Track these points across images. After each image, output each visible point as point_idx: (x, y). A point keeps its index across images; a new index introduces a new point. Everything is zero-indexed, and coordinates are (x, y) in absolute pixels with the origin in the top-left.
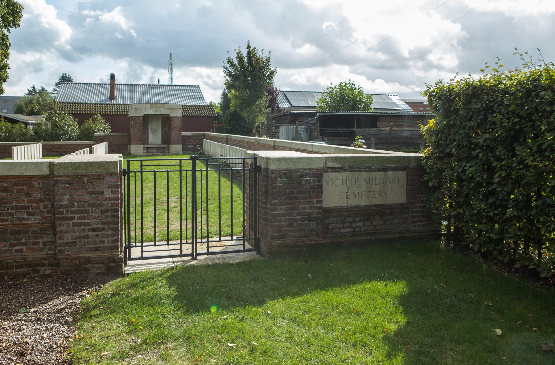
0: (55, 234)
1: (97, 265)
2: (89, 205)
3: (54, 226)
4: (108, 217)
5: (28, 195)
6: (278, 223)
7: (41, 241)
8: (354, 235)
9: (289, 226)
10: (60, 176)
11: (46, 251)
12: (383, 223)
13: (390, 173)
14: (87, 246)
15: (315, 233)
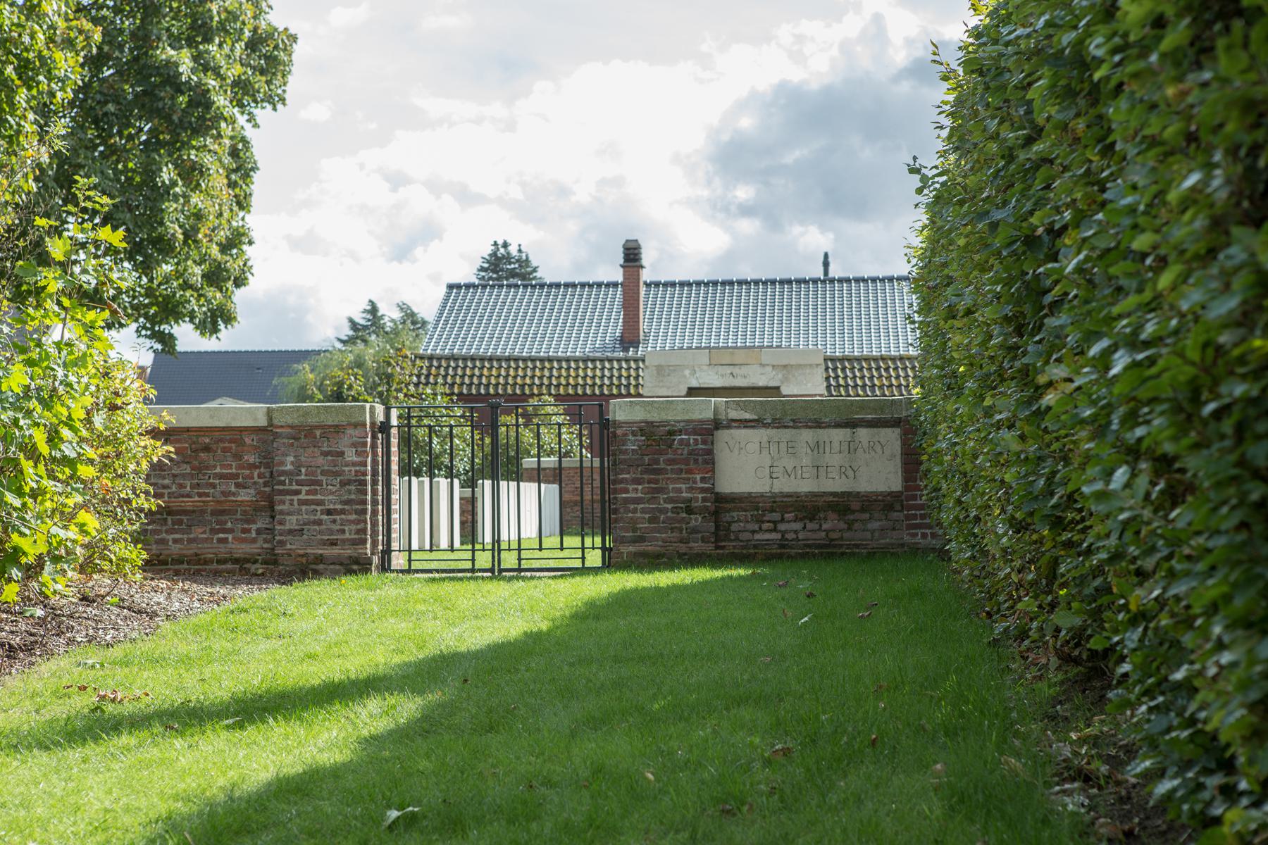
0: (273, 517)
1: (332, 567)
2: (323, 473)
3: (272, 507)
4: (349, 492)
5: (238, 457)
6: (630, 515)
7: (254, 527)
8: (782, 546)
9: (651, 520)
10: (282, 427)
11: (260, 543)
12: (845, 526)
13: (863, 433)
14: (319, 537)
15: (699, 536)
